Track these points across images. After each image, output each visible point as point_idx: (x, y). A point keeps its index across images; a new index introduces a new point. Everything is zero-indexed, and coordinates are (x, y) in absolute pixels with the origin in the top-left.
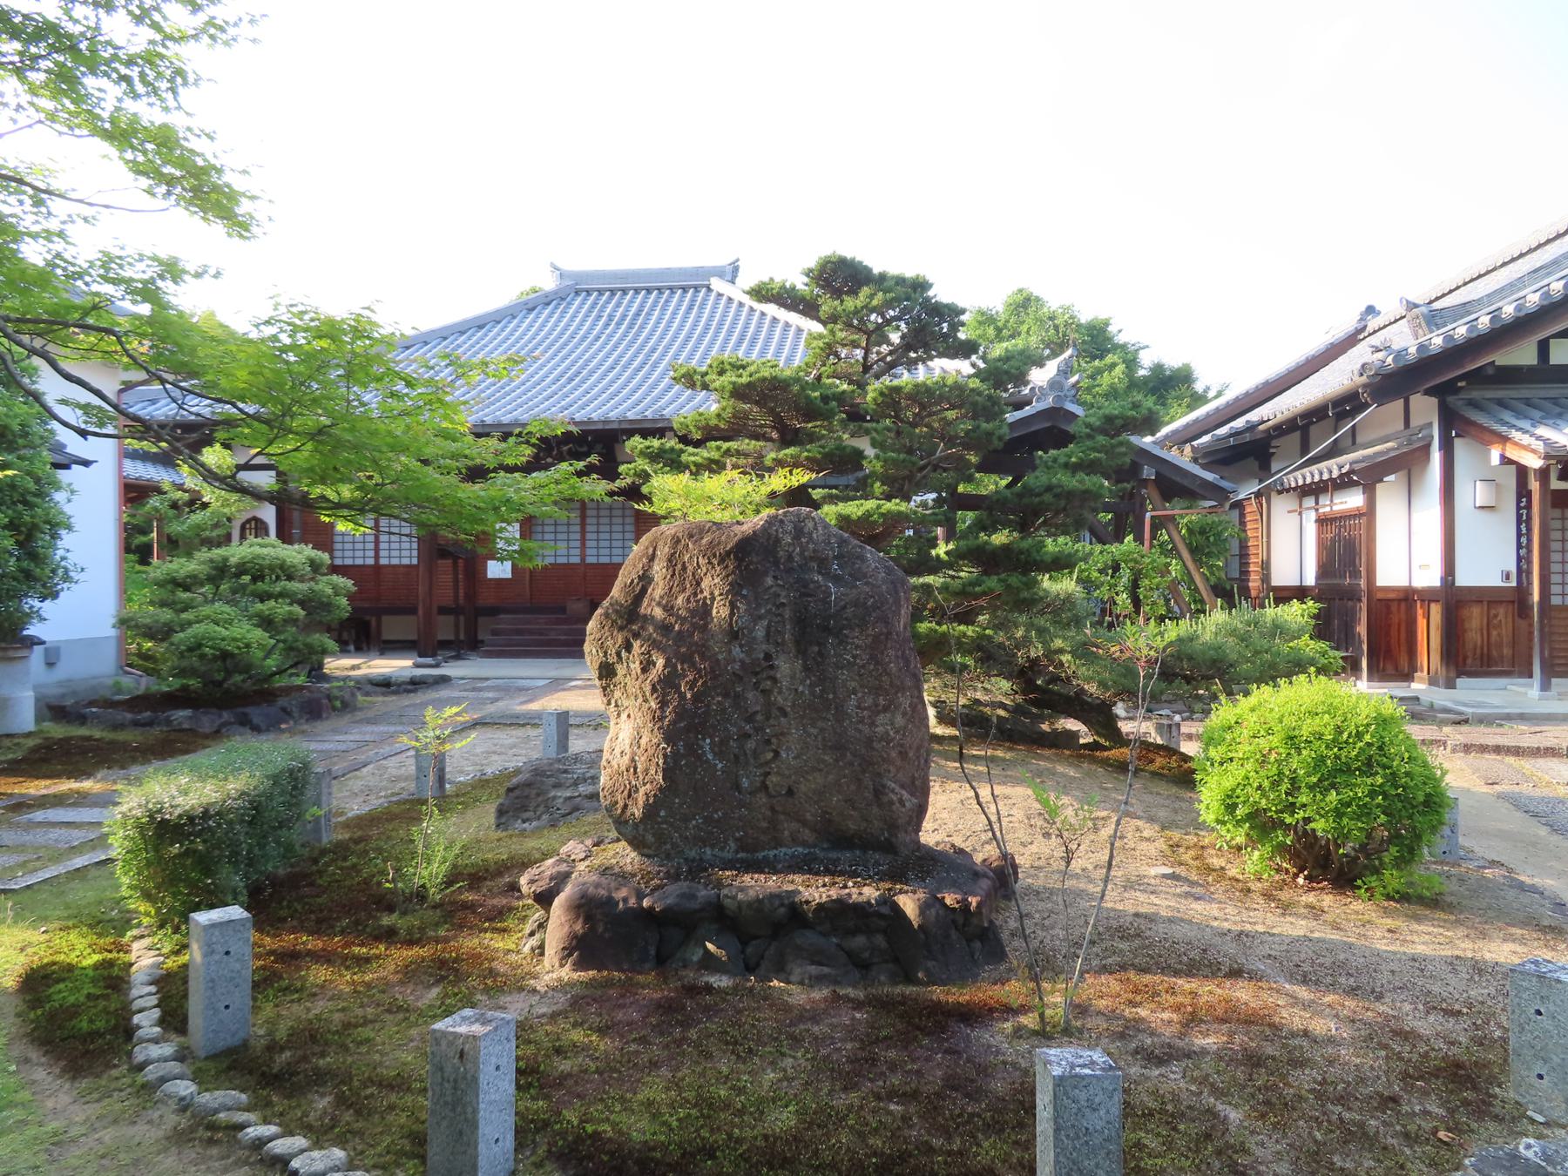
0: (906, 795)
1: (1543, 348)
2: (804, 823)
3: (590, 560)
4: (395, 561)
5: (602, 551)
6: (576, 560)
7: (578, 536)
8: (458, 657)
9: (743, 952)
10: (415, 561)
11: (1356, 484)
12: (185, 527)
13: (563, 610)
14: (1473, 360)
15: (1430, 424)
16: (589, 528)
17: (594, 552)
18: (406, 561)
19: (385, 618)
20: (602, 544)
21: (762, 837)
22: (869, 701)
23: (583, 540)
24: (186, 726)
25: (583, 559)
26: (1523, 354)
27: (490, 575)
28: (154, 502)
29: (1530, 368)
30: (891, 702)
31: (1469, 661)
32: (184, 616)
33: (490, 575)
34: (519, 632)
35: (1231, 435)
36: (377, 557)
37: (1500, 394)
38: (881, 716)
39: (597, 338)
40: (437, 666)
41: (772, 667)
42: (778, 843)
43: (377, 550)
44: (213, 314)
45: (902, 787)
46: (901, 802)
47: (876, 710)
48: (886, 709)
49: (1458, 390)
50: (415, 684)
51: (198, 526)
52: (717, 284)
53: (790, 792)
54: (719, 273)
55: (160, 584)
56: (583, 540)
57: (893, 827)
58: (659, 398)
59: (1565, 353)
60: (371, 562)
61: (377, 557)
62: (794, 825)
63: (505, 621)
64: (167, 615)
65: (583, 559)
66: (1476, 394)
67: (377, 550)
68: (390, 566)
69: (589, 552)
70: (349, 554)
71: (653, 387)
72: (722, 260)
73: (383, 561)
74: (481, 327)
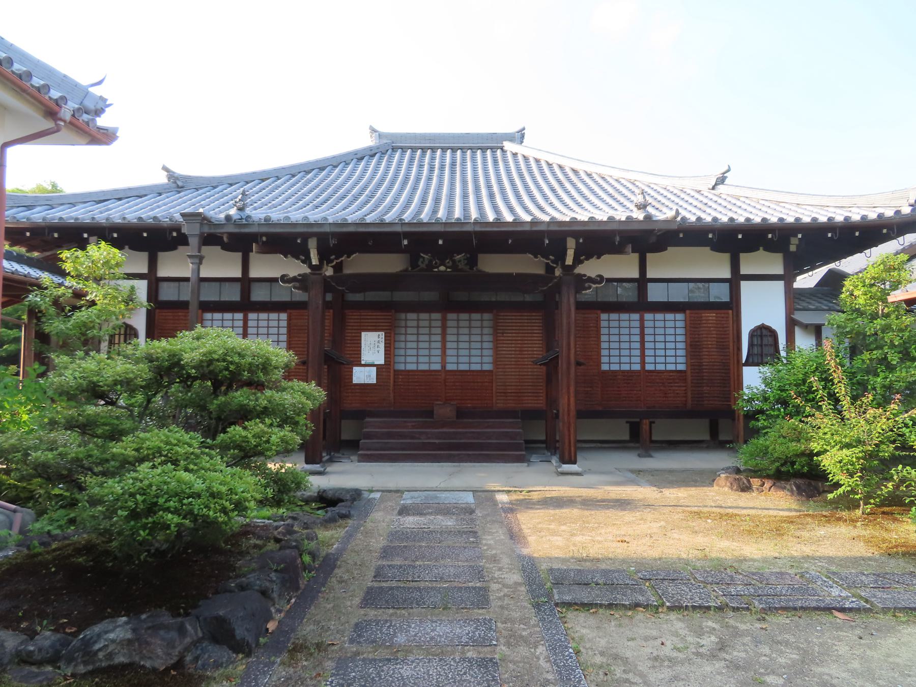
3: (450, 367)
5: (421, 359)
6: (437, 367)
7: (439, 345)
9: (419, 647)
10: (605, 367)
12: (69, 325)
13: (430, 414)
16: (449, 338)
17: (454, 359)
23: (444, 349)
24: (121, 659)
25: (444, 367)
27: (355, 380)
28: (33, 298)
32: (116, 448)
33: (355, 380)
34: (390, 435)
36: (643, 363)
44: (54, 186)
51: (85, 324)
52: (508, 146)
54: (511, 138)
55: (69, 395)
56: (444, 349)
61: (643, 363)
63: (373, 425)
64: (71, 443)
65: (444, 367)
69: (449, 359)
70: (627, 360)
72: (512, 129)
74: (322, 169)
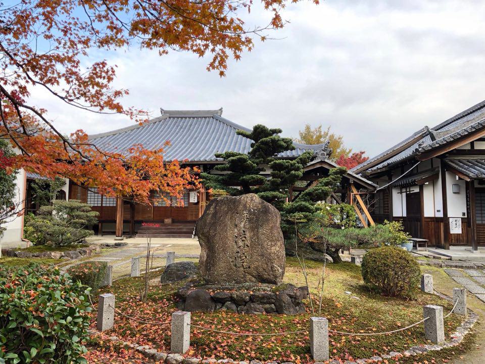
0: (279, 269)
1: (472, 144)
2: (253, 276)
4: (108, 205)
8: (130, 237)
11: (417, 185)
14: (435, 154)
15: (438, 167)
18: (111, 205)
19: (103, 224)
20: (97, 200)
21: (242, 280)
22: (270, 243)
26: (465, 145)
29: (468, 150)
30: (276, 244)
31: (453, 241)
35: (383, 167)
36: (102, 204)
37: (459, 158)
38: (273, 248)
39: (177, 134)
40: (122, 240)
41: (245, 234)
42: (246, 281)
43: (102, 201)
45: (278, 266)
46: (278, 270)
47: (272, 246)
48: (274, 245)
49: (446, 157)
50: (117, 245)
53: (249, 267)
57: (276, 277)
58: (199, 154)
59: (480, 146)
60: (100, 205)
61: (102, 204)
62: (250, 276)
66: (452, 158)
67: (102, 201)
68: (106, 207)
70: (93, 202)
71: (197, 150)
73: (104, 205)
